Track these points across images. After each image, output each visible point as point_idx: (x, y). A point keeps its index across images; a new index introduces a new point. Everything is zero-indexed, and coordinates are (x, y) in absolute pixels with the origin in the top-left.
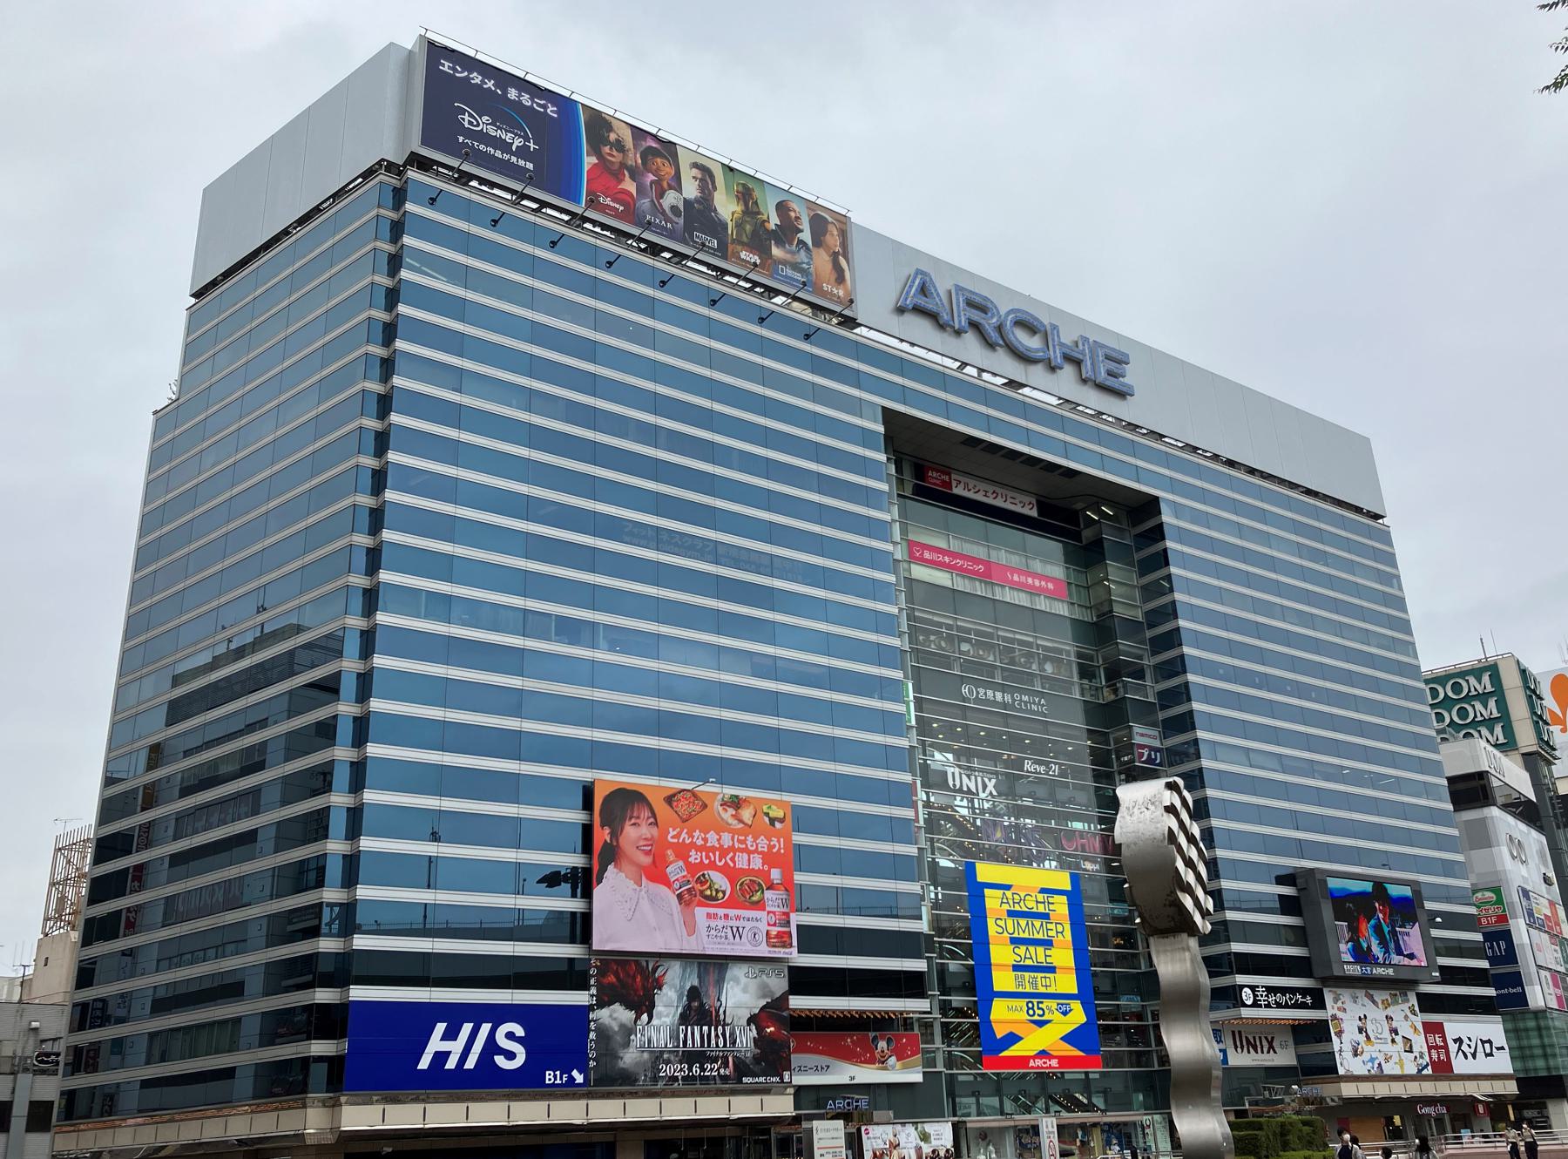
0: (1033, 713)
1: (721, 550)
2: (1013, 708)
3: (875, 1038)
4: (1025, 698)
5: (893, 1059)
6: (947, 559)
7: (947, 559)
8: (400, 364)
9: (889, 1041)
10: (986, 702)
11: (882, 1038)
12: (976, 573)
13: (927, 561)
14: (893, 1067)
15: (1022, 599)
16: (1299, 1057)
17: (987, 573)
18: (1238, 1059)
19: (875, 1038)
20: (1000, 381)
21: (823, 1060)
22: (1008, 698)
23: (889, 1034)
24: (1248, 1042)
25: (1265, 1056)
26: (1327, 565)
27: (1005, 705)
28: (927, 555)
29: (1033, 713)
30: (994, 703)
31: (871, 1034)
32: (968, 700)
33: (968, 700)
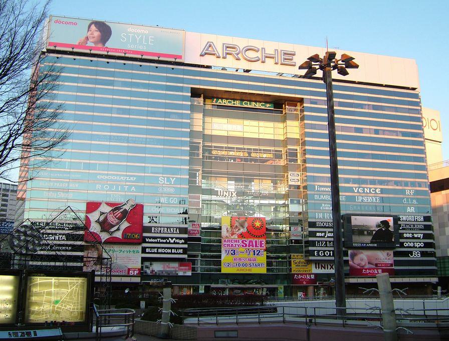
18: (315, 270)
24: (322, 266)
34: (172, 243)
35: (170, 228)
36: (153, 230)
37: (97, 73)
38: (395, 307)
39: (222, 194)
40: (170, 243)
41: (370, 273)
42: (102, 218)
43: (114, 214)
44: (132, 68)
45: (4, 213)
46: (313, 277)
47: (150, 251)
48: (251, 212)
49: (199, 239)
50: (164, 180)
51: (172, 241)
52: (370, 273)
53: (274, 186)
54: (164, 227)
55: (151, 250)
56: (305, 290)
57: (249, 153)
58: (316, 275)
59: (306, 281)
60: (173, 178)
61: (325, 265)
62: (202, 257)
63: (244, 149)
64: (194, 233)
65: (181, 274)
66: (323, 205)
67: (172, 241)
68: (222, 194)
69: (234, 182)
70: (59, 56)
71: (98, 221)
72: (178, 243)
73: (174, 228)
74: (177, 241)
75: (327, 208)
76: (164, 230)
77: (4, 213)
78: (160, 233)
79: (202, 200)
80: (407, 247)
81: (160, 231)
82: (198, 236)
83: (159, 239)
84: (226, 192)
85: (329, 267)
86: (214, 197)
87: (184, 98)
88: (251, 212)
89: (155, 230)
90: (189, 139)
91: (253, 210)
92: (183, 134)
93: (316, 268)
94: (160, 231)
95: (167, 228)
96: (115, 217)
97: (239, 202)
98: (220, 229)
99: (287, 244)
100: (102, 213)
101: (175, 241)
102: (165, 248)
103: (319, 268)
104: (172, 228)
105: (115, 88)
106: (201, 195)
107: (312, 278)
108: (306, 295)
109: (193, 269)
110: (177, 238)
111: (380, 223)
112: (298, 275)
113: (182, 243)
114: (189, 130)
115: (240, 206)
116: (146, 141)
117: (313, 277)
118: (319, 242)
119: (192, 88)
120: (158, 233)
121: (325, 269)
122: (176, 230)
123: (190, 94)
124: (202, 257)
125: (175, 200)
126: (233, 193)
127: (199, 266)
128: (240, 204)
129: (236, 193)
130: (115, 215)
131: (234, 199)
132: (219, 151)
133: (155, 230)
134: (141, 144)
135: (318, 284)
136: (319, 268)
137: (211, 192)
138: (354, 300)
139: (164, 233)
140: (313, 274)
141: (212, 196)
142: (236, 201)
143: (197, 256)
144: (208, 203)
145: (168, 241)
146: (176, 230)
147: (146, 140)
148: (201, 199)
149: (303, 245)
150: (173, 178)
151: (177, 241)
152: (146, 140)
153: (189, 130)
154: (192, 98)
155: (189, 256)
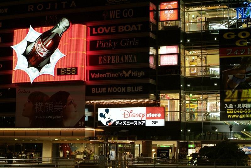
34: (127, 78)
36: (100, 60)
40: (124, 77)
42: (30, 49)
43: (43, 43)
45: (113, 29)
47: (97, 92)
51: (127, 75)
55: (134, 89)
65: (149, 123)
67: (127, 75)
71: (25, 54)
72: (136, 77)
74: (135, 74)
76: (115, 59)
77: (113, 29)
80: (139, 85)
83: (108, 74)
89: (103, 60)
96: (45, 46)
100: (29, 43)
101: (130, 74)
102: (117, 86)
110: (134, 70)
111: (90, 53)
113: (142, 77)
120: (107, 64)
122: (133, 57)
125: (131, 12)
130: (45, 43)
145: (121, 75)
146: (133, 57)
151: (135, 74)
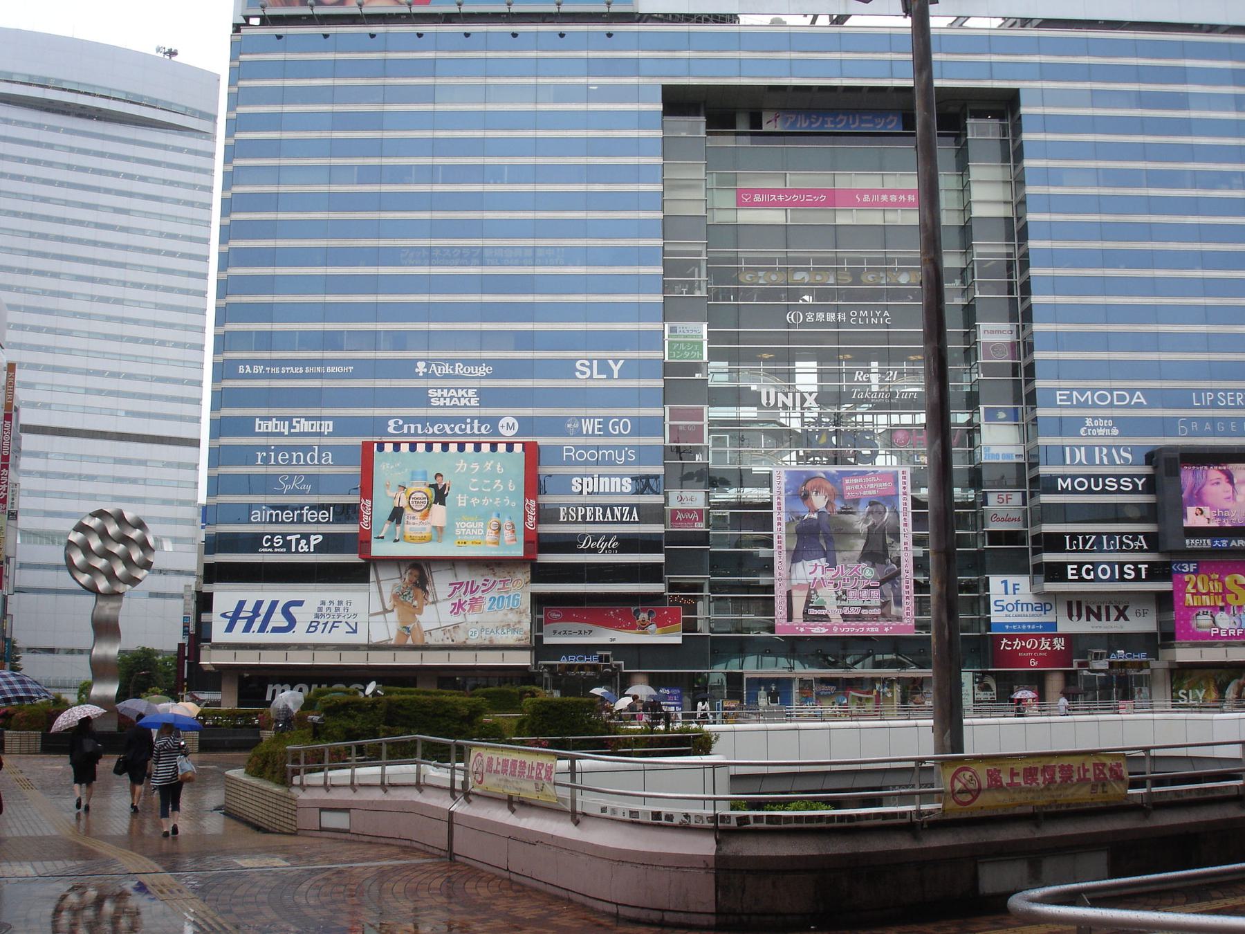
0: (874, 326)
1: (487, 253)
2: (848, 325)
3: (637, 611)
4: (863, 313)
5: (653, 627)
6: (781, 198)
7: (781, 198)
8: (1026, 150)
9: (650, 613)
10: (817, 324)
11: (644, 611)
12: (819, 204)
13: (757, 204)
14: (653, 632)
15: (875, 218)
16: (1160, 624)
17: (833, 199)
18: (1067, 626)
19: (637, 611)
20: (997, 22)
21: (587, 627)
22: (842, 316)
23: (651, 608)
24: (1089, 611)
25: (1112, 622)
26: (1231, 188)
27: (838, 324)
28: (757, 198)
29: (874, 326)
30: (825, 324)
31: (633, 608)
32: (794, 326)
33: (794, 326)
35: (612, 507)
36: (562, 514)
37: (385, 68)
38: (949, 788)
39: (772, 402)
41: (1023, 649)
44: (537, 42)
46: (1059, 644)
48: (866, 452)
49: (703, 538)
50: (591, 367)
52: (1023, 649)
53: (730, 372)
54: (594, 506)
56: (1037, 681)
57: (856, 275)
58: (1069, 638)
59: (1037, 659)
60: (616, 361)
61: (1099, 608)
62: (714, 587)
63: (839, 261)
64: (689, 520)
66: (1089, 422)
68: (772, 402)
69: (814, 364)
70: (377, 29)
73: (622, 505)
75: (1101, 432)
78: (584, 521)
79: (711, 423)
81: (584, 516)
82: (700, 527)
84: (786, 395)
85: (1114, 614)
86: (748, 412)
87: (641, 120)
88: (866, 452)
89: (568, 513)
90: (660, 242)
91: (871, 444)
92: (641, 228)
93: (1070, 616)
94: (584, 516)
95: (604, 507)
97: (827, 424)
98: (769, 505)
99: (980, 545)
103: (1079, 616)
104: (617, 506)
105: (439, 107)
106: (705, 407)
107: (1058, 647)
108: (1041, 697)
109: (690, 626)
112: (1011, 638)
114: (660, 215)
115: (830, 435)
116: (534, 257)
117: (1059, 644)
118: (1074, 536)
119: (666, 89)
121: (1099, 619)
122: (630, 513)
123: (660, 107)
124: (714, 587)
125: (625, 425)
126: (806, 395)
127: (703, 612)
128: (832, 429)
129: (814, 395)
131: (811, 415)
132: (761, 274)
133: (568, 513)
134: (522, 265)
135: (1075, 667)
136: (1079, 616)
137: (738, 397)
138: (1150, 716)
139: (594, 522)
140: (1060, 636)
141: (742, 409)
142: (818, 422)
143: (698, 587)
144: (738, 432)
146: (630, 513)
147: (534, 252)
148: (706, 419)
149: (1029, 546)
150: (616, 361)
152: (534, 252)
153: (660, 215)
154: (667, 118)
155: (673, 587)
